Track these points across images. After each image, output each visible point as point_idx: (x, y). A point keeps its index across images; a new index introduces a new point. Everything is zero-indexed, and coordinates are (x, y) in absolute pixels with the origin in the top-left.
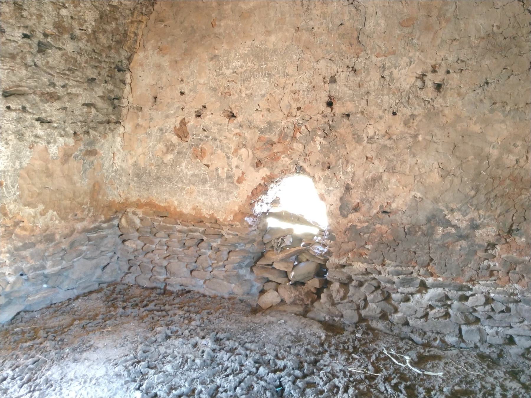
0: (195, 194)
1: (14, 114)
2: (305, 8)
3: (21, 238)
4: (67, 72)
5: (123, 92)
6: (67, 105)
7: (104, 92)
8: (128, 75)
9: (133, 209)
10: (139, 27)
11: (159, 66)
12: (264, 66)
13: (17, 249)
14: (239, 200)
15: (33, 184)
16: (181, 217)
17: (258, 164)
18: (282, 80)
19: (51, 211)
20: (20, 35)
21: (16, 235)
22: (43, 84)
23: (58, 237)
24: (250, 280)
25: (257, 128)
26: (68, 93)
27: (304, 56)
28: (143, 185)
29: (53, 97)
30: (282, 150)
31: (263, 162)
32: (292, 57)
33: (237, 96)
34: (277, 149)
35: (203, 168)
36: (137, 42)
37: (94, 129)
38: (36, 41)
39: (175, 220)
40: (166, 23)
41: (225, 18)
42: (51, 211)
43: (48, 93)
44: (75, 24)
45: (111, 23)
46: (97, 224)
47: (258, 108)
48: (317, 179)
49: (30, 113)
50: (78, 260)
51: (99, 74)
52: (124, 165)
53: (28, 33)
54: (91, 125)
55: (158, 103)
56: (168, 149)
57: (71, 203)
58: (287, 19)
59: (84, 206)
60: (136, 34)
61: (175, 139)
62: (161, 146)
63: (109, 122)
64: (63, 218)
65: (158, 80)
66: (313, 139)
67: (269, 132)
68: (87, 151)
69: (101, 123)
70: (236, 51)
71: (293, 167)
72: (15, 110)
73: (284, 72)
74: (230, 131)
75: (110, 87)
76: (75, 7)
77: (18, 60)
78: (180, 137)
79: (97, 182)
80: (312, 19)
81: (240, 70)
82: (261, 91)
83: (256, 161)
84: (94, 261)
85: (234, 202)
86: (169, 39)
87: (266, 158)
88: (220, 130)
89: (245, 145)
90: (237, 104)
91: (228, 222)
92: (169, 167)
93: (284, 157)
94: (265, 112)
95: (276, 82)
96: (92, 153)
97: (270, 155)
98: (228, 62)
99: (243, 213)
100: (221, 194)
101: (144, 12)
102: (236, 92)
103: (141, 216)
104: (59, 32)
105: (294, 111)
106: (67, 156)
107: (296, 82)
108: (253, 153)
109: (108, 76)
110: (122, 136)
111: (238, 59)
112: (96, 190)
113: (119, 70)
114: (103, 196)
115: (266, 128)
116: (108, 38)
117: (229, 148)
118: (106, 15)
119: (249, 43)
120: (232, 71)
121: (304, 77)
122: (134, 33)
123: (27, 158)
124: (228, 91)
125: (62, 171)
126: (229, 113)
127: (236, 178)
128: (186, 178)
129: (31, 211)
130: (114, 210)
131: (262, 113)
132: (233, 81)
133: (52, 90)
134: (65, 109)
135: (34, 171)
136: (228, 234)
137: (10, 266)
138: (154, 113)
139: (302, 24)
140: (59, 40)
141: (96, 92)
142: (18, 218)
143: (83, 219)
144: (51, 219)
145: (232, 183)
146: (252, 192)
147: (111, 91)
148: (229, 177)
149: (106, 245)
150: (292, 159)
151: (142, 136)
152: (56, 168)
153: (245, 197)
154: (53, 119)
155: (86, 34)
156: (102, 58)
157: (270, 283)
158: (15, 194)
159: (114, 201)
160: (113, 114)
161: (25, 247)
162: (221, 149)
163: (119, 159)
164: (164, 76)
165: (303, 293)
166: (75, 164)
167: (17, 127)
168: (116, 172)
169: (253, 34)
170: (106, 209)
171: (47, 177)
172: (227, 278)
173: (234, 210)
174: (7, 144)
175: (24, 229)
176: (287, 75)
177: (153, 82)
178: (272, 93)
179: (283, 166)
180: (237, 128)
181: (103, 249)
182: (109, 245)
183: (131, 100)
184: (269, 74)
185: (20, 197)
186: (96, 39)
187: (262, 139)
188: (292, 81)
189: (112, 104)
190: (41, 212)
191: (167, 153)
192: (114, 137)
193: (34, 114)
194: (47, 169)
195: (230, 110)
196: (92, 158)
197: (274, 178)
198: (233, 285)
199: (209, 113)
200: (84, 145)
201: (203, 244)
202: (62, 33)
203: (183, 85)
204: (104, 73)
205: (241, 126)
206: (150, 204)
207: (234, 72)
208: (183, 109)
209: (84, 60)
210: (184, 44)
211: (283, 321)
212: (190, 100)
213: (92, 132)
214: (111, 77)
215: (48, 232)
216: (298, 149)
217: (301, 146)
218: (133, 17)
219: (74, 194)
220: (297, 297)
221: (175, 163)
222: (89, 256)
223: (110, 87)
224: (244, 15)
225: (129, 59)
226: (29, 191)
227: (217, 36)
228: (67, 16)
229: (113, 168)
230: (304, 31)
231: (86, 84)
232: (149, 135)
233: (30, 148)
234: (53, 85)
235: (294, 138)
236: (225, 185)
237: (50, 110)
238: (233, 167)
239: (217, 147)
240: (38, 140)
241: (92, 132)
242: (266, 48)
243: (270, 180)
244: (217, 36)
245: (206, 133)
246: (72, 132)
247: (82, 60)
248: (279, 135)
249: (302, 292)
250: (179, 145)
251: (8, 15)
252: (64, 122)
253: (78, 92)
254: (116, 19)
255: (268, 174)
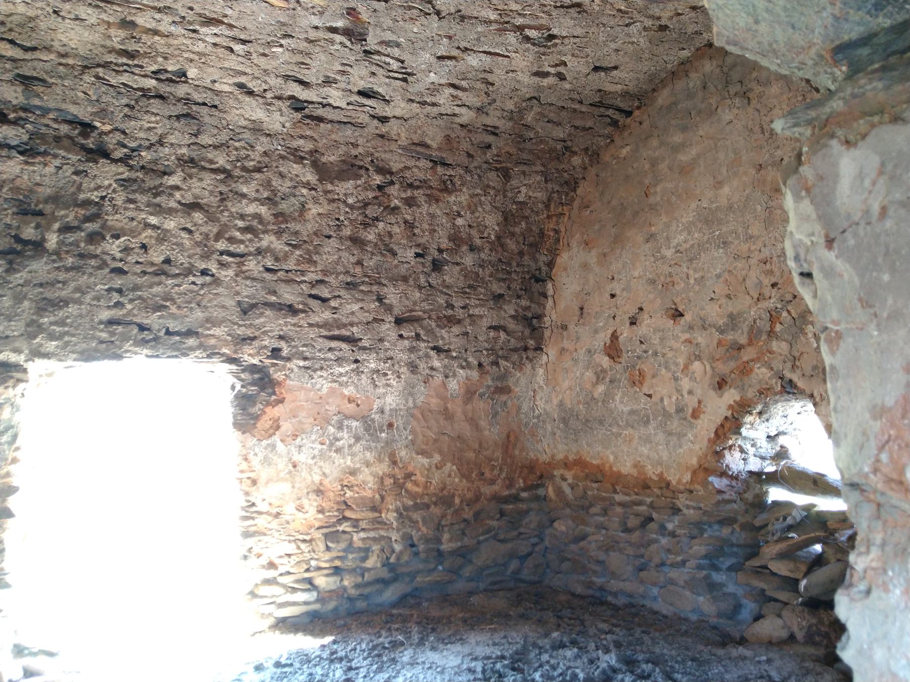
0: (636, 441)
1: (406, 343)
2: (767, 134)
3: (412, 496)
4: (467, 290)
5: (544, 308)
6: (469, 329)
7: (516, 311)
8: (550, 285)
9: (562, 471)
10: (561, 220)
11: (585, 266)
12: (717, 233)
13: (406, 508)
14: (697, 447)
15: (428, 428)
16: (616, 480)
17: (721, 385)
18: (744, 247)
19: (449, 465)
20: (413, 254)
21: (407, 491)
22: (440, 306)
23: (457, 501)
24: (735, 595)
25: (714, 326)
26: (469, 315)
27: (772, 204)
28: (571, 434)
29: (452, 321)
30: (755, 356)
31: (729, 380)
32: (755, 210)
33: (683, 285)
34: (748, 354)
35: (644, 399)
36: (559, 241)
37: (506, 358)
38: (430, 258)
39: (613, 485)
40: (591, 208)
41: (661, 180)
42: (449, 465)
43: (445, 316)
44: (474, 232)
45: (520, 223)
46: (513, 491)
47: (713, 296)
48: (818, 399)
49: (424, 341)
50: (486, 540)
51: (509, 288)
52: (548, 407)
53: (421, 252)
54: (500, 353)
55: (585, 315)
56: (598, 378)
57: (476, 457)
58: (744, 158)
59: (493, 463)
60: (557, 232)
61: (605, 361)
62: (589, 375)
63: (526, 349)
64: (464, 476)
65: (584, 285)
66: (802, 331)
67: (733, 330)
68: (497, 388)
69: (515, 350)
70: (678, 221)
71: (776, 383)
72: (408, 338)
73: (746, 234)
74: (676, 338)
75: (524, 303)
76: (473, 213)
77: (411, 282)
78: (613, 358)
79: (513, 430)
80: (778, 147)
81: (685, 246)
82: (715, 269)
83: (717, 379)
84: (509, 545)
85: (691, 450)
86: (596, 228)
87: (732, 372)
88: (662, 339)
89: (699, 356)
90: (683, 296)
91: (685, 485)
92: (600, 404)
93: (759, 368)
94: (724, 301)
95: (735, 251)
96: (504, 390)
97: (738, 367)
98: (668, 239)
99: (706, 470)
100: (670, 438)
101: (564, 201)
102: (681, 279)
103: (570, 481)
104: (455, 245)
105: (767, 291)
106: (470, 394)
107: (765, 246)
108: (712, 368)
109: (521, 289)
110: (544, 366)
111: (682, 231)
112: (509, 441)
113: (538, 280)
114: (521, 451)
115: (727, 325)
116: (518, 242)
117: (677, 364)
118: (512, 215)
119: (693, 205)
120: (673, 250)
121: (777, 235)
122: (554, 230)
123: (422, 394)
124: (671, 279)
125: (465, 413)
126: (673, 311)
127: (690, 410)
128: (622, 419)
129: (425, 461)
130: (538, 473)
131: (719, 302)
132: (676, 264)
133: (450, 312)
134: (466, 334)
135: (430, 411)
136: (688, 507)
137: (398, 530)
138: (580, 330)
139: (765, 159)
140: (456, 254)
141: (505, 311)
142: (410, 469)
143: (492, 482)
144: (450, 476)
145: (685, 419)
146: (716, 433)
147: (527, 308)
148: (680, 410)
149: (526, 524)
150: (772, 369)
151: (568, 364)
152: (456, 407)
153: (705, 442)
154: (452, 348)
155: (488, 242)
156: (511, 268)
157: (772, 603)
158: (406, 438)
159: (537, 460)
160: (531, 339)
161: (416, 507)
162: (666, 368)
163: (541, 399)
164: (591, 277)
165: (827, 623)
166: (481, 404)
167: (410, 358)
168: (538, 417)
169: (698, 192)
170: (526, 471)
171: (446, 419)
172: (691, 584)
173: (692, 465)
174: (399, 377)
175: (416, 483)
176: (751, 237)
177: (579, 289)
178: (731, 269)
179: (760, 382)
180: (686, 332)
181: (522, 530)
182: (532, 526)
183: (554, 317)
184: (724, 243)
185: (413, 442)
186: (502, 246)
187: (724, 343)
188: (759, 244)
189: (530, 325)
190: (436, 464)
191: (597, 384)
192: (533, 368)
193: (429, 342)
194: (446, 409)
195: (673, 307)
196: (504, 398)
197: (749, 406)
198: (701, 599)
199: (646, 316)
200: (493, 379)
201: (652, 526)
202: (459, 246)
203: (615, 284)
204: (516, 286)
205: (691, 328)
206: (580, 463)
207: (677, 252)
208: (614, 317)
209: (487, 272)
210: (614, 230)
211: (764, 658)
212: (623, 303)
213: (502, 362)
214: (525, 290)
215: (445, 492)
216: (779, 351)
217: (784, 345)
218: (549, 210)
219: (480, 444)
220: (814, 628)
221: (608, 396)
222: (502, 537)
223: (524, 303)
224: (685, 171)
225: (551, 264)
226: (424, 436)
227: (653, 208)
228: (464, 226)
229: (534, 412)
230: (770, 168)
231: (491, 302)
232: (576, 361)
233: (425, 382)
234: (451, 306)
235: (771, 333)
236: (674, 425)
237: (449, 336)
238: (685, 393)
239: (660, 366)
240: (434, 373)
241: (502, 362)
242: (717, 207)
243: (742, 408)
244: (653, 208)
245: (644, 347)
246: (476, 363)
247: (485, 273)
248: (748, 333)
249: (826, 619)
250: (611, 370)
251: (399, 236)
252: (466, 350)
253: (482, 313)
254: (527, 217)
255: (738, 398)
